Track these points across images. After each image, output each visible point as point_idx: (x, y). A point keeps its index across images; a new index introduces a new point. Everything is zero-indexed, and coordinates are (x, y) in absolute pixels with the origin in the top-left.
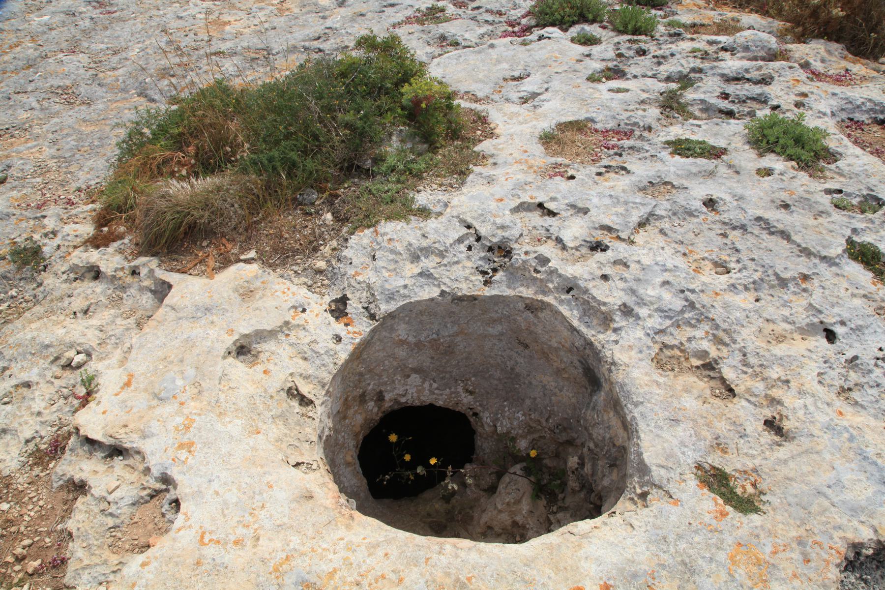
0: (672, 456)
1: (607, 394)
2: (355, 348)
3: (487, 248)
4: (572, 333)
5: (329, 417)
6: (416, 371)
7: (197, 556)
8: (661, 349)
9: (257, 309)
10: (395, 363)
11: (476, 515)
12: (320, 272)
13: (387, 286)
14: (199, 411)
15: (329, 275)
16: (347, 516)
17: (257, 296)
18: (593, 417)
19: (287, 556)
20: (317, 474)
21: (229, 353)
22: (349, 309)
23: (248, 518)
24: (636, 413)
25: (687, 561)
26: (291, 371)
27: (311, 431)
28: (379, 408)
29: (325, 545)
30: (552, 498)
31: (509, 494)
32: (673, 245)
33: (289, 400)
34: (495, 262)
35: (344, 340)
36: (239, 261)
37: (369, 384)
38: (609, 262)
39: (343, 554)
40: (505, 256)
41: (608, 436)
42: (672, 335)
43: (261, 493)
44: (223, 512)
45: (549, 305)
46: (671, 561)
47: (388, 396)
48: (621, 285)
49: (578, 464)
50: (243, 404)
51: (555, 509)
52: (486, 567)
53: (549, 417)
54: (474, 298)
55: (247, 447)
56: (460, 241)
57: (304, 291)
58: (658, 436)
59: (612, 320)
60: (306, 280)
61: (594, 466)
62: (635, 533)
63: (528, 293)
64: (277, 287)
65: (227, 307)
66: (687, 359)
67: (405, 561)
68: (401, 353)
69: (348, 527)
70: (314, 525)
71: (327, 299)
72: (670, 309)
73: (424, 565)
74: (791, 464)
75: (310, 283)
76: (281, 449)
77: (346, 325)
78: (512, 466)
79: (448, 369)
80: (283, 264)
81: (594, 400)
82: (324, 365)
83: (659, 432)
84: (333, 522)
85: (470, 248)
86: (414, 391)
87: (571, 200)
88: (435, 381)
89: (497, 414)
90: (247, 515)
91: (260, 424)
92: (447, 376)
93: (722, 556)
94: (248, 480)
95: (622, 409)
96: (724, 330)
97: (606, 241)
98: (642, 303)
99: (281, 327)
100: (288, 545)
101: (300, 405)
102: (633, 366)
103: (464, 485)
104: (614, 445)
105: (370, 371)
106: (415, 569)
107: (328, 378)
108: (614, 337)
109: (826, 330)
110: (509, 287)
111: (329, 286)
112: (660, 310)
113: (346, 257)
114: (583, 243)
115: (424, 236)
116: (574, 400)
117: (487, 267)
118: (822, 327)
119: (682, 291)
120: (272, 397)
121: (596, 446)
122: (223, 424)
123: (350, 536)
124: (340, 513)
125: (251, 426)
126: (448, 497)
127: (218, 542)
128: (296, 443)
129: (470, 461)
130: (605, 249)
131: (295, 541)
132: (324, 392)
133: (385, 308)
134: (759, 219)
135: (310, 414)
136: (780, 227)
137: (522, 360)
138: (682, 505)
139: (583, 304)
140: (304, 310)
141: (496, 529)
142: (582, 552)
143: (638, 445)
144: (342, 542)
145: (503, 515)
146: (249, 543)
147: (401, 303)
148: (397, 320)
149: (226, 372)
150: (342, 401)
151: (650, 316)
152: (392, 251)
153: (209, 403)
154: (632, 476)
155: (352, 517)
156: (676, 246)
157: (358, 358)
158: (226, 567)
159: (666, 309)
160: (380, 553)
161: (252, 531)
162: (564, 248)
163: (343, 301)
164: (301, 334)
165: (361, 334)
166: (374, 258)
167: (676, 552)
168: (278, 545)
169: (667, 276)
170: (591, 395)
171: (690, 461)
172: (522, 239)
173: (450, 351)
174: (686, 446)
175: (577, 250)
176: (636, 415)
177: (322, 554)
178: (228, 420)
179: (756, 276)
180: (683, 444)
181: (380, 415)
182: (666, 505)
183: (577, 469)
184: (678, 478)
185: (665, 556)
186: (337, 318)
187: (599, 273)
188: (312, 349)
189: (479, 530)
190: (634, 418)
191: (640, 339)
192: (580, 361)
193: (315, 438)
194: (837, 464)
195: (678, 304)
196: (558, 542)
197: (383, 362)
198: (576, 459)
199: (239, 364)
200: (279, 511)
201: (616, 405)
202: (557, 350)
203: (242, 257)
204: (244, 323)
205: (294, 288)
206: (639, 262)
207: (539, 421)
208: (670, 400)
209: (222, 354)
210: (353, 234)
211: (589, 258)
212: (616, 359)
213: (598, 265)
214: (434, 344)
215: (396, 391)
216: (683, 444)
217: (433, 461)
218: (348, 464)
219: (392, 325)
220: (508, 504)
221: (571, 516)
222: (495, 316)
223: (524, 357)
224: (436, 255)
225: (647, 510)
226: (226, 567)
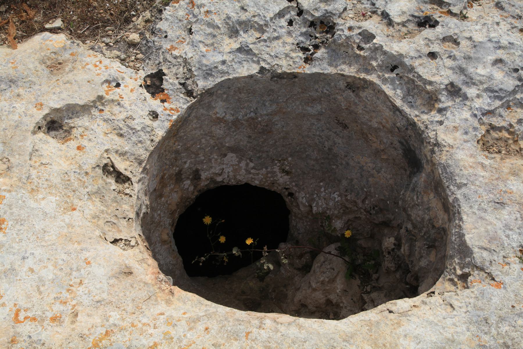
0: (495, 239)
1: (428, 175)
2: (172, 125)
3: (308, 23)
4: (394, 113)
5: (146, 195)
6: (232, 149)
7: (11, 334)
8: (488, 131)
9: (68, 82)
10: (212, 142)
11: (290, 293)
12: (133, 45)
13: (205, 61)
14: (8, 188)
15: (143, 49)
16: (167, 291)
17: (67, 69)
18: (413, 199)
19: (107, 332)
20: (136, 250)
21: (39, 128)
22: (165, 85)
23: (65, 295)
24: (459, 194)
25: (510, 343)
26: (106, 148)
27: (129, 208)
28: (195, 187)
29: (145, 320)
30: (366, 278)
31: (324, 273)
32: (510, 20)
33: (105, 177)
34: (316, 38)
35: (161, 117)
36: (43, 30)
37: (185, 163)
38: (438, 39)
39: (164, 328)
40: (327, 32)
41: (427, 217)
42: (501, 116)
43: (78, 270)
44: (38, 290)
45: (372, 83)
46: (492, 343)
48: (449, 63)
49: (395, 244)
50: (56, 180)
51: (368, 288)
52: (305, 342)
53: (366, 198)
54: (294, 76)
55: (63, 224)
56: (281, 14)
57: (117, 64)
58: (481, 218)
59: (438, 100)
60: (118, 53)
61: (411, 247)
62: (455, 313)
63: (349, 70)
64: (88, 59)
65: (33, 79)
66: (516, 142)
67: (225, 335)
68: (218, 131)
69: (168, 302)
70: (133, 300)
71: (142, 74)
72: (501, 89)
73: (244, 339)
75: (123, 56)
76: (98, 226)
77: (163, 101)
78: (328, 245)
79: (265, 149)
80: (93, 35)
81: (413, 181)
82: (140, 142)
83: (483, 215)
84: (153, 298)
85: (290, 23)
86: (229, 170)
88: (251, 161)
89: (313, 195)
90: (64, 291)
91: (76, 201)
92: (264, 155)
94: (64, 257)
95: (444, 190)
97: (436, 16)
98: (470, 82)
99: (94, 102)
100: (108, 321)
101: (117, 181)
102: (458, 148)
103: (278, 264)
104: (434, 227)
105: (187, 149)
106: (236, 343)
107: (145, 155)
108: (438, 118)
110: (330, 65)
111: (144, 60)
112: (489, 90)
113: (160, 30)
114: (411, 18)
115: (242, 8)
116: (391, 182)
117: (308, 43)
119: (516, 70)
120: (87, 173)
121: (415, 226)
122: (36, 201)
123: (170, 311)
124: (160, 288)
125: (66, 202)
126: (263, 276)
127: (34, 319)
128: (114, 220)
129: (284, 241)
130: (434, 24)
131: (115, 316)
132: (141, 170)
133: (202, 84)
135: (128, 191)
137: (340, 141)
138: (505, 288)
139: (408, 83)
140: (118, 85)
141: (310, 307)
142: (401, 329)
143: (460, 226)
144: (162, 317)
145: (317, 293)
146: (67, 319)
147: (219, 80)
148: (214, 97)
149: (36, 148)
150: (158, 178)
151: (478, 96)
152: (210, 25)
153: (20, 179)
154: (452, 257)
155: (172, 293)
156: (513, 21)
157: (175, 135)
158: (43, 344)
159: (496, 88)
160: (201, 327)
161: (70, 307)
162: (390, 23)
163: (159, 76)
164: (116, 109)
165: (178, 111)
166: (190, 32)
167: (498, 334)
168: (97, 320)
169: (500, 54)
170: (410, 177)
171: (515, 245)
172: (345, 14)
173: (267, 130)
174: (511, 230)
175: (404, 26)
176: (459, 196)
177: (142, 329)
178: (41, 196)
180: (507, 227)
181: (196, 193)
182: (487, 287)
183: (393, 250)
184: (501, 261)
185: (486, 338)
186: (153, 94)
187: (426, 50)
188: (128, 126)
189: (294, 308)
190: (456, 200)
191: (467, 120)
192: (400, 142)
193: (132, 215)
196: (376, 319)
197: (200, 140)
198: (392, 240)
199: (50, 140)
200: (98, 287)
201: (438, 187)
202: (376, 130)
203: (47, 26)
204: (53, 97)
205: (107, 62)
206: (470, 39)
207: (355, 202)
208: (495, 182)
209: (32, 128)
210: (167, 4)
211: (416, 35)
212: (439, 139)
213: (426, 41)
214: (252, 122)
215: (213, 170)
216: (507, 227)
217: (249, 241)
218: (164, 242)
219: (210, 103)
220: (323, 283)
221: (385, 296)
222: (314, 94)
223: (343, 138)
224: (256, 30)
225: (467, 291)
226: (43, 344)
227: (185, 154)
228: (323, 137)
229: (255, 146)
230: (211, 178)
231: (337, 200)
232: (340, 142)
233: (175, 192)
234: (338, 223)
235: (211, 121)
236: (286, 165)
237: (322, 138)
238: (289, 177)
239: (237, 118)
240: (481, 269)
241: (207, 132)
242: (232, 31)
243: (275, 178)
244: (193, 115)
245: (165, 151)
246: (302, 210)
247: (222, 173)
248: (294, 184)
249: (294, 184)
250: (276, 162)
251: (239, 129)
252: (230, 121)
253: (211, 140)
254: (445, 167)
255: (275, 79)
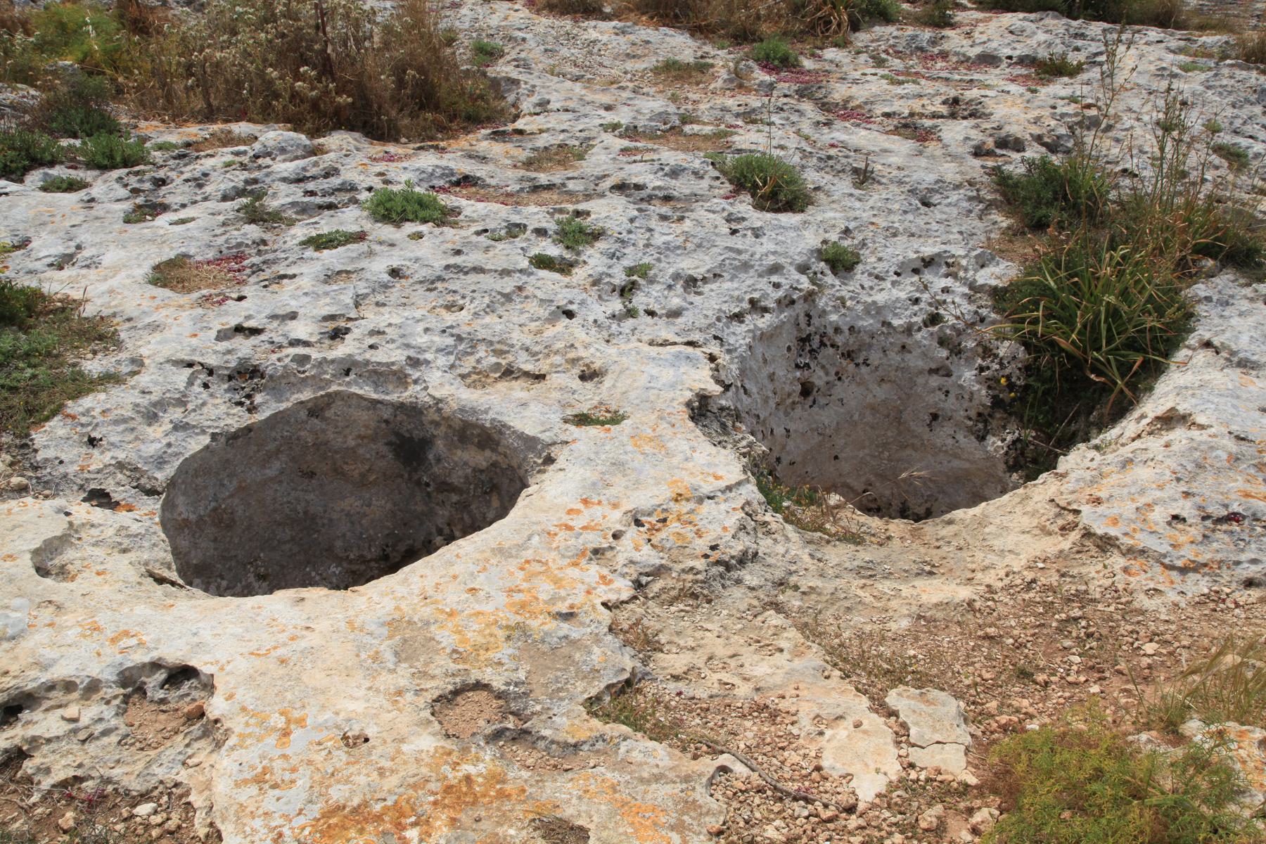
4: (375, 409)
34: (243, 388)
45: (337, 393)
54: (249, 429)
56: (190, 383)
63: (306, 395)
74: (618, 385)
85: (206, 386)
87: (268, 312)
88: (223, 579)
92: (233, 563)
93: (629, 448)
96: (499, 342)
109: (564, 312)
116: (389, 506)
118: (560, 312)
119: (444, 331)
134: (447, 267)
136: (470, 265)
179: (487, 300)
185: (599, 468)
194: (643, 368)
195: (450, 341)
240: (554, 443)
242: (149, 418)
254: (462, 410)
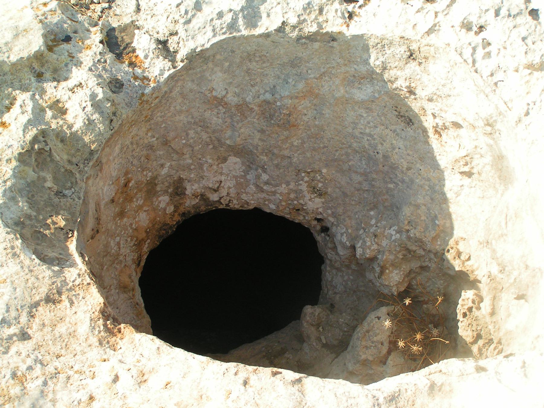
37: (162, 166)
47: (190, 189)
79: (286, 153)
104: (527, 267)
129: (314, 302)
137: (401, 144)
148: (210, 65)
181: (177, 218)
215: (204, 182)
227: (161, 153)
228: (375, 137)
229: (270, 147)
230: (202, 195)
231: (393, 238)
232: (401, 146)
233: (145, 211)
234: (393, 274)
235: (204, 102)
236: (319, 181)
237: (374, 139)
238: (323, 200)
239: (244, 100)
241: (197, 120)
243: (301, 202)
244: (178, 89)
245: (132, 143)
246: (341, 253)
247: (218, 187)
248: (329, 212)
249: (329, 212)
250: (303, 175)
251: (246, 118)
252: (233, 104)
253: (203, 133)
255: (304, 40)
